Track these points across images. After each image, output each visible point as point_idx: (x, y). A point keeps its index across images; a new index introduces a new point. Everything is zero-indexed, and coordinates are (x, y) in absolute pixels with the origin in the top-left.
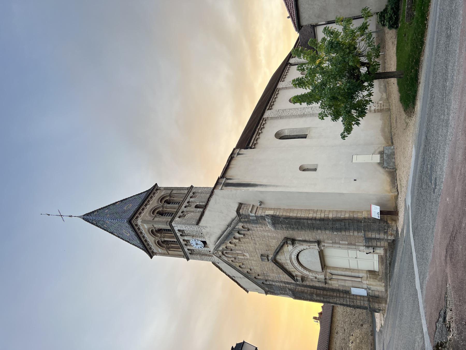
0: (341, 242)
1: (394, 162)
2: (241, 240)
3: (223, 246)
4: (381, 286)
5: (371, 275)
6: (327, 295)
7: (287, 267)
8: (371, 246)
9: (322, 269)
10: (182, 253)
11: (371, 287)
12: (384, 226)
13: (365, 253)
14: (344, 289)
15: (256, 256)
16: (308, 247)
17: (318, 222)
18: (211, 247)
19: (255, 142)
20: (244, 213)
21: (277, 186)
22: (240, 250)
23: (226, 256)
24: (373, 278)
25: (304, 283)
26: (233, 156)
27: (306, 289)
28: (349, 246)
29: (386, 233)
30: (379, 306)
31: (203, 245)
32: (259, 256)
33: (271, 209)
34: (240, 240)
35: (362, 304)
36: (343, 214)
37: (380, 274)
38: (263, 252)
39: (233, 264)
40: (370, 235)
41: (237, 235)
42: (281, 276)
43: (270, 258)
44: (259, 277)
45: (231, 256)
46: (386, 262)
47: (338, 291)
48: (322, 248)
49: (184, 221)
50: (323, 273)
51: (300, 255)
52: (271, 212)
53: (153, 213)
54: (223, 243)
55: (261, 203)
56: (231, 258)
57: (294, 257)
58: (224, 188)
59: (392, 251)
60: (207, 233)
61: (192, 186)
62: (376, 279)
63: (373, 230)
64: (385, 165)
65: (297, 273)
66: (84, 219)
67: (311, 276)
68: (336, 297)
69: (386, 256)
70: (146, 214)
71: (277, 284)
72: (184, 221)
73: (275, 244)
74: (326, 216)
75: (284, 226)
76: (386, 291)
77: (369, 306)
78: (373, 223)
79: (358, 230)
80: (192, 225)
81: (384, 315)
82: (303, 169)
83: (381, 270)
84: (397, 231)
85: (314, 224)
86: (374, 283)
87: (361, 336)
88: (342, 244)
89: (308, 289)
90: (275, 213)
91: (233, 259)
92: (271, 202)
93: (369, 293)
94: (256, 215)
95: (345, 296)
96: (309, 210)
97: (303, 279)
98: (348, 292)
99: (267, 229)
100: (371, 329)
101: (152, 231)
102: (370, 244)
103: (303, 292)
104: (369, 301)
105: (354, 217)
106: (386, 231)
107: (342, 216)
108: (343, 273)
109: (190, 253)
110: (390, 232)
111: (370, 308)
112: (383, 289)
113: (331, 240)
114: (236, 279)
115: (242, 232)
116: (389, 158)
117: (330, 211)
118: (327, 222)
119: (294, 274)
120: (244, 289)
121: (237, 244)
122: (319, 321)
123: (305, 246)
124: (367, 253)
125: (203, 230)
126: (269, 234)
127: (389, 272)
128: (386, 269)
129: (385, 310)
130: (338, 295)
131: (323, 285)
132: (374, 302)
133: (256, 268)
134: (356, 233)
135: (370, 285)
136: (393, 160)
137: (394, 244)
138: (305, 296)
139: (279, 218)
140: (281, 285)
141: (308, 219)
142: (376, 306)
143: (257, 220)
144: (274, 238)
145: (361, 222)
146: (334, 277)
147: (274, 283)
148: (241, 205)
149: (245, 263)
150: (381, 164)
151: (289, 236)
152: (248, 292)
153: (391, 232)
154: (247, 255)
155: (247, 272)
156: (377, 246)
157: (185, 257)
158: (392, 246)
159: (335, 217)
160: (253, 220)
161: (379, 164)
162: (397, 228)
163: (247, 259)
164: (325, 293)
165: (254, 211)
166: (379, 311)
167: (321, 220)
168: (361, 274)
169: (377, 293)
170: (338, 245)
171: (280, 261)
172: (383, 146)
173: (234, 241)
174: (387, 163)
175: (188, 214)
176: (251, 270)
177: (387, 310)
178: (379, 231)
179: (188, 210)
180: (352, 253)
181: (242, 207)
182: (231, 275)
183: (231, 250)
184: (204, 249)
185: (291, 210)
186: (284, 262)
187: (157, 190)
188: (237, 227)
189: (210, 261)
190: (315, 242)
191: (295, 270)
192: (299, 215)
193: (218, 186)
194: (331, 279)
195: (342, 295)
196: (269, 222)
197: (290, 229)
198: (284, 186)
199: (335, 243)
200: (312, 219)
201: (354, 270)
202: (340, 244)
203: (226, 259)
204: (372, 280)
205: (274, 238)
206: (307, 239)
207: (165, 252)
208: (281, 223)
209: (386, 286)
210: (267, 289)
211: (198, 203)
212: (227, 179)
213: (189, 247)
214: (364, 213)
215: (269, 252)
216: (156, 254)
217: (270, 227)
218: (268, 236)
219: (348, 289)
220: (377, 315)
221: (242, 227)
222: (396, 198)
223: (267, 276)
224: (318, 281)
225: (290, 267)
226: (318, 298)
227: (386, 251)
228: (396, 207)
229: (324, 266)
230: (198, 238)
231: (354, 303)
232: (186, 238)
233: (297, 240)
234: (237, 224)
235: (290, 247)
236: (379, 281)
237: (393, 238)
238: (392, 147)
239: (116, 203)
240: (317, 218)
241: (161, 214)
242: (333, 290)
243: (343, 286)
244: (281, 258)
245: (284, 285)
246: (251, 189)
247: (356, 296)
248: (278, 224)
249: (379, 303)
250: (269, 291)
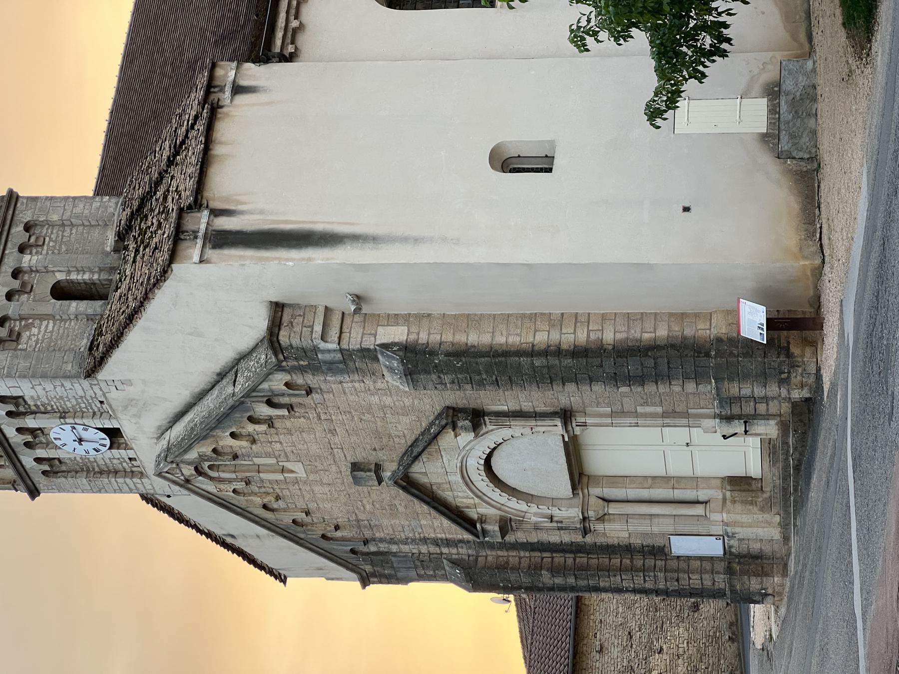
0: (640, 409)
1: (814, 133)
2: (277, 424)
3: (206, 448)
4: (769, 523)
5: (736, 494)
6: (587, 568)
7: (448, 495)
8: (739, 417)
9: (574, 488)
10: (9, 473)
11: (737, 530)
12: (780, 364)
13: (719, 436)
14: (648, 542)
15: (334, 468)
16: (527, 431)
17: (568, 361)
18: (145, 447)
19: (294, 24)
20: (295, 342)
21: (416, 241)
22: (268, 455)
23: (211, 479)
24: (744, 502)
25: (510, 538)
26: (213, 97)
27: (513, 556)
28: (666, 421)
29: (784, 382)
30: (762, 583)
31: (107, 442)
32: (346, 469)
33: (394, 319)
34: (271, 425)
35: (708, 583)
36: (649, 325)
37: (767, 488)
38: (360, 456)
39: (241, 501)
40: (734, 389)
41: (264, 410)
42: (424, 522)
43: (387, 474)
44: (339, 534)
45: (233, 476)
46: (786, 459)
47: (627, 549)
48: (578, 430)
49: (23, 364)
50: (575, 500)
51: (495, 453)
52: (397, 334)
54: (205, 438)
55: (358, 299)
56: (230, 481)
57: (475, 463)
58: (210, 253)
59: (804, 433)
60: (129, 403)
62: (751, 503)
63: (744, 377)
64: (785, 144)
65: (484, 510)
67: (535, 514)
68: (621, 570)
69: (785, 443)
71: (405, 548)
72: (23, 364)
73: (406, 428)
74: (593, 336)
75: (447, 379)
76: (786, 539)
77: (732, 586)
78: (745, 355)
79: (699, 377)
80: (65, 377)
81: (777, 609)
82: (507, 163)
83: (770, 476)
84: (818, 377)
85: (553, 366)
86: (745, 519)
87: (692, 650)
88: (646, 416)
89: (522, 554)
90: (413, 337)
91: (240, 486)
92: (390, 296)
93: (730, 547)
94: (344, 346)
95: (650, 562)
96: (533, 317)
97: (505, 525)
98: (659, 552)
99: (379, 385)
100: (730, 617)
102: (735, 414)
103: (503, 567)
104: (730, 571)
105: (685, 338)
106: (783, 376)
107: (646, 336)
108: (645, 494)
109: (44, 473)
110: (796, 379)
111: (733, 591)
112: (775, 533)
113: (609, 405)
114: (238, 543)
115: (285, 400)
116: (797, 115)
117: (604, 317)
118: (597, 361)
119: (473, 514)
120: (271, 572)
121: (262, 438)
122: (511, 597)
123: (518, 428)
124: (725, 437)
125: (113, 395)
126: (388, 401)
127: (796, 490)
128: (785, 478)
129: (780, 594)
130: (627, 562)
131: (578, 538)
132: (744, 573)
133: (328, 506)
134: (691, 387)
135: (735, 524)
136: (811, 123)
137: (810, 412)
138: (513, 577)
139: (433, 353)
140: (424, 549)
141: (532, 353)
142: (754, 584)
143: (344, 362)
144: (405, 412)
145: (707, 355)
146: (613, 509)
147: (394, 548)
148: (277, 308)
149: (286, 493)
150: (768, 139)
151: (461, 403)
152: (284, 581)
153: (799, 378)
154: (298, 468)
155: (294, 521)
156: (756, 416)
157: (22, 486)
158: (805, 416)
159: (621, 341)
160: (331, 363)
161: (764, 138)
162: (818, 369)
163: (296, 481)
164: (582, 560)
165: (334, 333)
166: (761, 597)
167: (579, 353)
168: (705, 491)
169: (755, 547)
170: (634, 421)
171: (423, 480)
172: (779, 56)
173: (251, 428)
174: (792, 136)
175: (28, 327)
176: (308, 513)
177: (790, 598)
178: (763, 377)
179: (25, 311)
180: (677, 434)
181: (286, 318)
182: (218, 531)
183: (235, 457)
184: (109, 454)
185: (471, 320)
186: (439, 481)
188: (265, 386)
189: (131, 491)
190: (552, 415)
191: (477, 500)
192: (500, 340)
193: (183, 246)
194: (601, 519)
195: (639, 563)
196: (391, 369)
197: (469, 387)
198: (444, 240)
199: (622, 413)
200: (545, 353)
201: (679, 479)
202: (636, 415)
203: (211, 487)
204: (739, 507)
205: (405, 412)
206: (526, 406)
208: (439, 370)
209: (784, 526)
210: (368, 568)
211: (60, 276)
212: (216, 213)
213: (41, 453)
214: (714, 316)
215: (382, 456)
217: (394, 381)
218: (383, 407)
219: (659, 542)
220: (757, 611)
221: (287, 384)
222: (818, 273)
223: (371, 527)
224: (559, 529)
225: (460, 497)
226: (558, 581)
227: (784, 427)
228: (817, 302)
229: (578, 475)
230: (86, 421)
231: (682, 582)
232: (30, 422)
233: (490, 414)
234: (266, 377)
235: (466, 437)
236: (762, 510)
237: (808, 395)
238: (810, 64)
240: (564, 347)
242: (610, 550)
243: (645, 535)
244: (428, 471)
245: (433, 549)
246: (318, 256)
247: (689, 558)
248: (428, 373)
249: (764, 573)
250: (374, 575)
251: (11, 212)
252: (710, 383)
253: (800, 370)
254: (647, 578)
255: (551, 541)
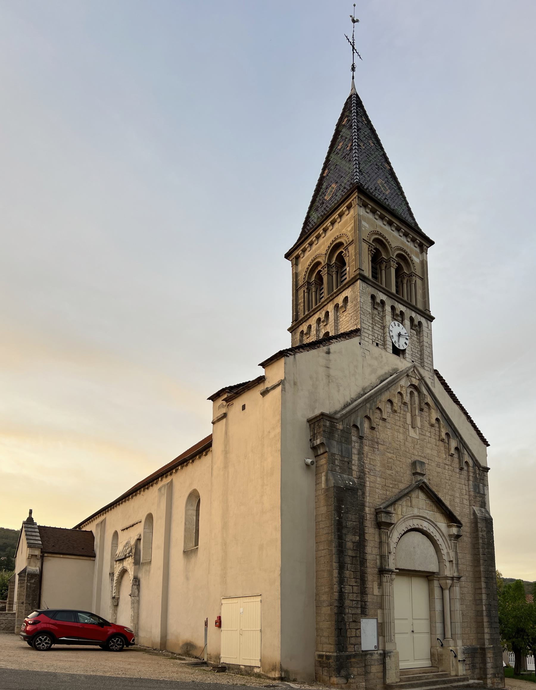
36: (371, 586)
53: (376, 240)
61: (433, 318)
66: (350, 97)
70: (372, 224)
101: (340, 244)
110: (496, 680)
153: (496, 681)
187: (421, 246)
207: (301, 283)
216: (295, 264)
239: (389, 163)
241: (376, 260)
251: (383, 291)
252: (489, 645)
253: (500, 681)
254: (354, 602)
255: (368, 547)
